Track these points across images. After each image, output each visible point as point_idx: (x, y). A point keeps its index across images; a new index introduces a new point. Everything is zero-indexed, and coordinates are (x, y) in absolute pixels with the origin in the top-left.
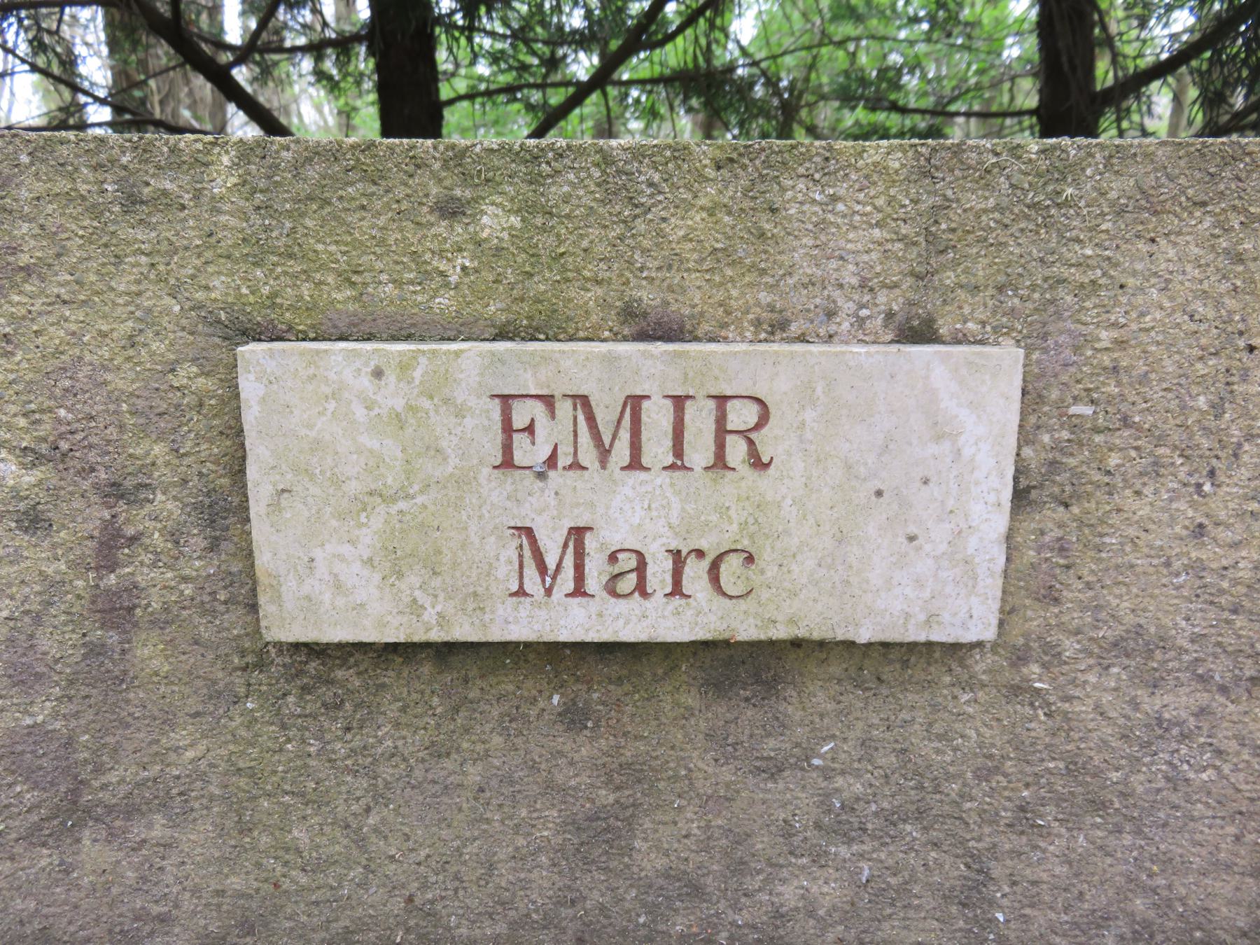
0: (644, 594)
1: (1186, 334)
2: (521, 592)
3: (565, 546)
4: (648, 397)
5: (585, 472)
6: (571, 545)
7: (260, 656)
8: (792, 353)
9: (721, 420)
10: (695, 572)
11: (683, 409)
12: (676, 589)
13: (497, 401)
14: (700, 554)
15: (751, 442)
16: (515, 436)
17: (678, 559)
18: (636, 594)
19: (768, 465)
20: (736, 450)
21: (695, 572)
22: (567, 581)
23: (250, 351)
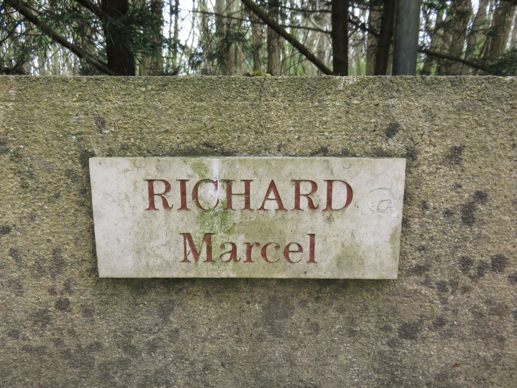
0: (236, 261)
1: (464, 146)
2: (186, 260)
3: (185, 243)
4: (252, 180)
5: (189, 212)
6: (187, 241)
7: (99, 281)
8: (245, 159)
9: (297, 190)
10: (256, 253)
11: (331, 185)
12: (249, 259)
13: (294, 182)
14: (258, 244)
15: (309, 198)
16: (233, 196)
17: (249, 247)
18: (232, 261)
19: (171, 208)
20: (304, 203)
21: (256, 253)
22: (204, 255)
23: (401, 164)
